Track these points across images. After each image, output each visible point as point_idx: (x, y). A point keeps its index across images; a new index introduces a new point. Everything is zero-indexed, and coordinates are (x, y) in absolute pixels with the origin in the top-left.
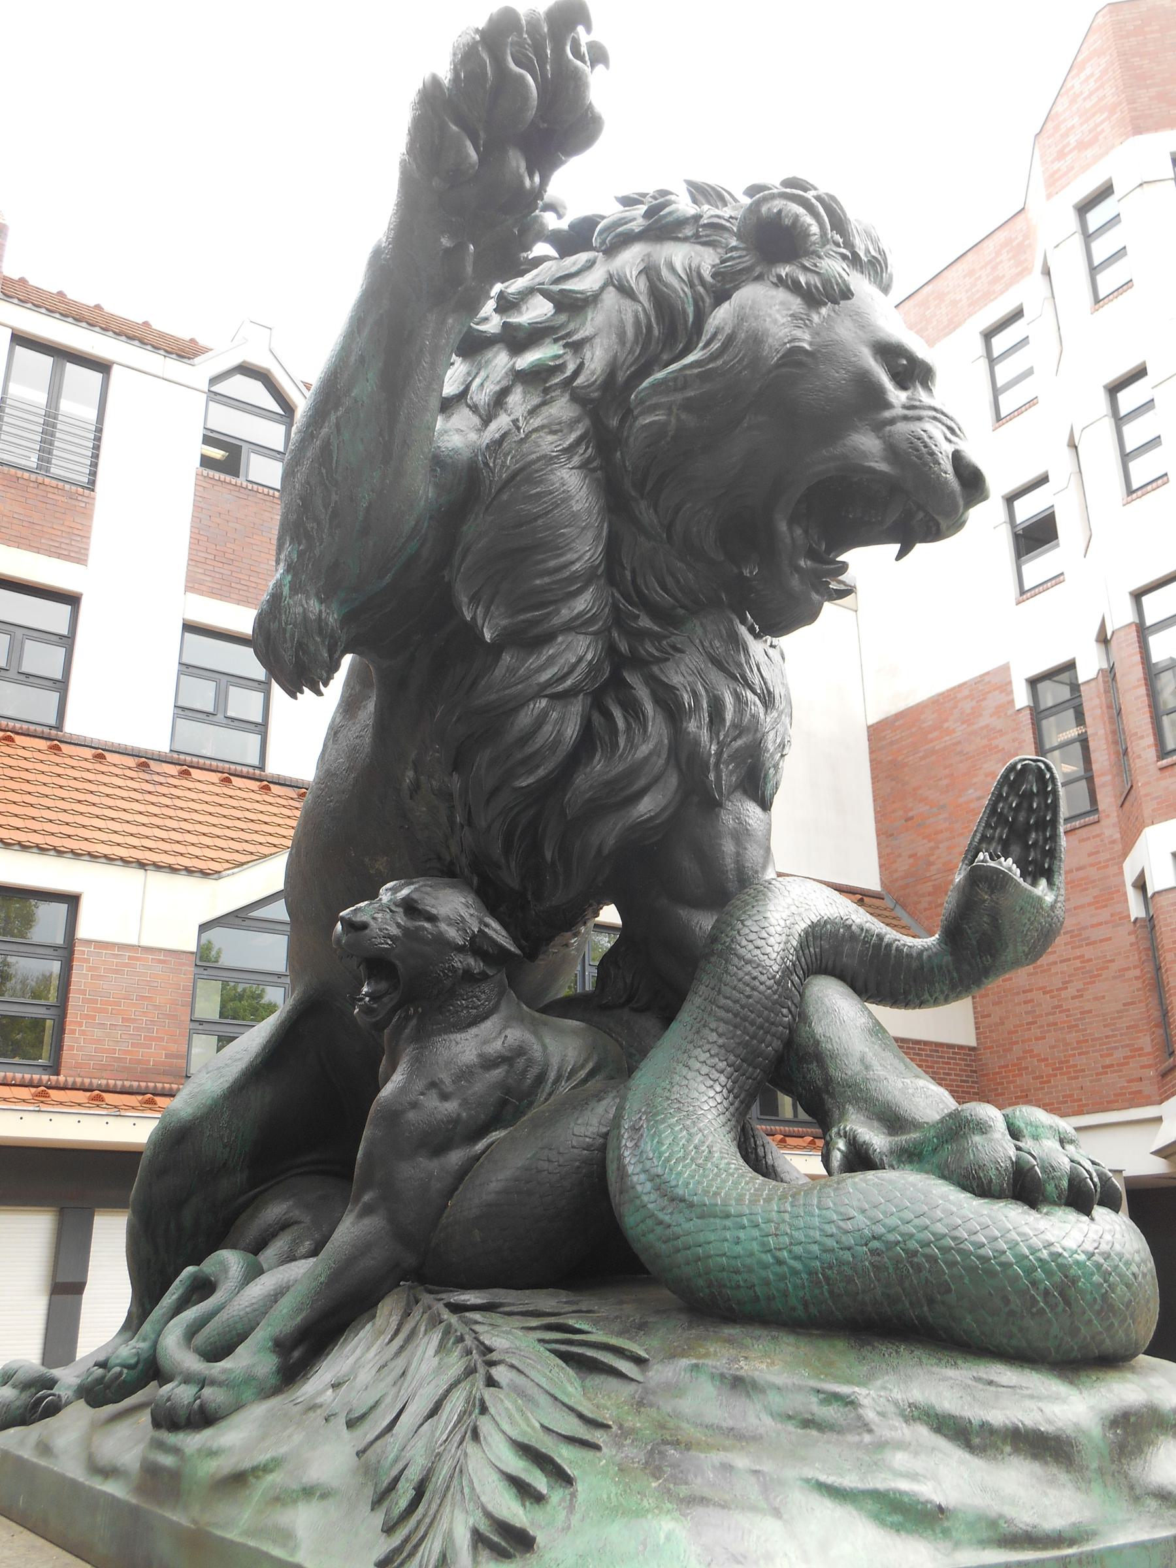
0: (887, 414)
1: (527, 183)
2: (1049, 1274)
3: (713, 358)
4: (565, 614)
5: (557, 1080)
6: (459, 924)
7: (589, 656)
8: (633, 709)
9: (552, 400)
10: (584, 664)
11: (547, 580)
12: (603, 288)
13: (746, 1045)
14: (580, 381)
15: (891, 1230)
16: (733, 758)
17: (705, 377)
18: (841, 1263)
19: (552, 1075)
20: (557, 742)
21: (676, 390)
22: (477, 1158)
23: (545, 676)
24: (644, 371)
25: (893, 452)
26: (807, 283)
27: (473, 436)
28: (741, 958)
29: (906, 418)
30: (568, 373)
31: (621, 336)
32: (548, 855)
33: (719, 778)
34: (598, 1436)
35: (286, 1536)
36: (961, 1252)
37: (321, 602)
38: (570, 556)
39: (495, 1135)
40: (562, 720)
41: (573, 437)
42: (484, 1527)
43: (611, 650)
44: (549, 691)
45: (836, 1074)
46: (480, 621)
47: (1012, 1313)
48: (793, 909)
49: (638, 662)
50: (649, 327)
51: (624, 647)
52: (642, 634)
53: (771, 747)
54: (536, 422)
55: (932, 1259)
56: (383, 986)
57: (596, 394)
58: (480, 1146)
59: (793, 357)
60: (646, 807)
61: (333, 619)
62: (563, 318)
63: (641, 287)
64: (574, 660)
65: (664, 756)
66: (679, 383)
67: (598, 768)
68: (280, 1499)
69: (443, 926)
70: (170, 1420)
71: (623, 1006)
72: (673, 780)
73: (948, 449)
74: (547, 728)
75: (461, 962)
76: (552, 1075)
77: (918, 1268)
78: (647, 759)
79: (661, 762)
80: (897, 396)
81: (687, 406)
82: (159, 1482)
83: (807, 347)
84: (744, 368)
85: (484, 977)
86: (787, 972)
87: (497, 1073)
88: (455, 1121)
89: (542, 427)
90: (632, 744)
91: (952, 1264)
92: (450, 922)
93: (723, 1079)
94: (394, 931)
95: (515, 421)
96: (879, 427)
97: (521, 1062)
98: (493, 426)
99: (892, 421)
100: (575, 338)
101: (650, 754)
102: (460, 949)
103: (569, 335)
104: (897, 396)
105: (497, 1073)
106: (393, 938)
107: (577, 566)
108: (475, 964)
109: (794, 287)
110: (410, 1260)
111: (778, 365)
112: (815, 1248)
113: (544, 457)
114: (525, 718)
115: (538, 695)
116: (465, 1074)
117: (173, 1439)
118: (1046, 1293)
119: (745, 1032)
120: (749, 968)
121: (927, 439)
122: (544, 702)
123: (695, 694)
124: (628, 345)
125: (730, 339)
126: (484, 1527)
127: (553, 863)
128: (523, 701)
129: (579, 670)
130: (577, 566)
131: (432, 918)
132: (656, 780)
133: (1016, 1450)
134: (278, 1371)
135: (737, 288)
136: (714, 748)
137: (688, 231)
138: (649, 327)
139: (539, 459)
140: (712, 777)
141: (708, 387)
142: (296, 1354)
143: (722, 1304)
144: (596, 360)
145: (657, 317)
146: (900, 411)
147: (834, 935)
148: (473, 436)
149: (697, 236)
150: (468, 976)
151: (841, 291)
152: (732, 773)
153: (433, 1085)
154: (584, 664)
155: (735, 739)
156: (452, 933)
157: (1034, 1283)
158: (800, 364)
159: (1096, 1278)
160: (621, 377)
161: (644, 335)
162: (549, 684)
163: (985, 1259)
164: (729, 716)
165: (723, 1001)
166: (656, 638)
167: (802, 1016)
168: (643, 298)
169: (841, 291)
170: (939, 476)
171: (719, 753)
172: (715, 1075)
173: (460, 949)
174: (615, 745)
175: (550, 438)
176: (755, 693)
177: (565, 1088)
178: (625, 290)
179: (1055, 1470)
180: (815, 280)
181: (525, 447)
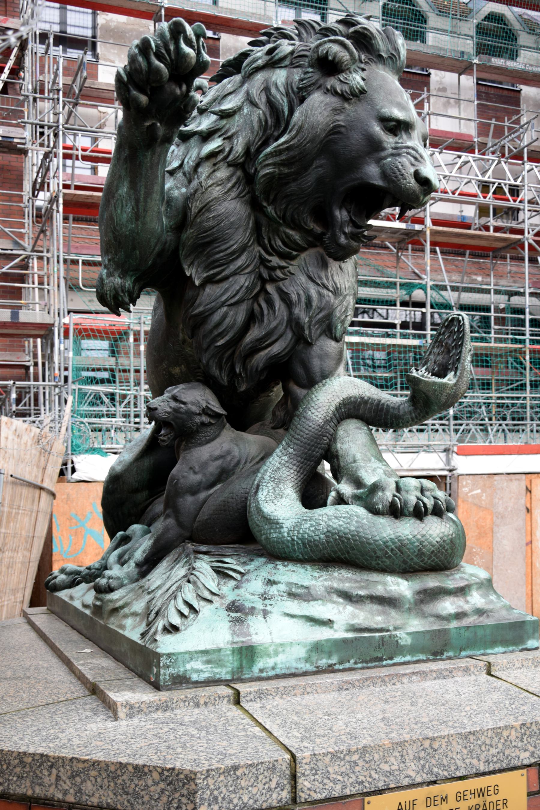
0: (383, 154)
1: (178, 92)
2: (394, 543)
3: (293, 138)
4: (233, 267)
5: (246, 463)
6: (197, 404)
7: (246, 284)
8: (270, 303)
9: (218, 169)
10: (244, 289)
11: (222, 254)
12: (243, 103)
13: (306, 453)
14: (230, 158)
15: (334, 529)
16: (317, 323)
17: (287, 149)
18: (314, 540)
19: (243, 461)
20: (232, 327)
21: (276, 156)
22: (211, 495)
23: (224, 298)
24: (265, 143)
25: (384, 175)
26: (341, 91)
27: (184, 190)
28: (305, 418)
29: (393, 155)
30: (225, 153)
31: (252, 128)
32: (238, 371)
33: (310, 332)
34: (215, 599)
35: (123, 627)
36: (359, 536)
37: (121, 278)
38: (231, 243)
39: (219, 486)
40: (236, 314)
41: (230, 185)
42: (167, 625)
43: (260, 277)
44: (228, 303)
45: (342, 464)
46: (193, 276)
47: (377, 557)
48: (334, 394)
49: (273, 280)
50: (266, 121)
51: (265, 275)
52: (274, 269)
53: (338, 314)
54: (210, 182)
55: (348, 539)
56: (168, 431)
57: (241, 160)
58: (212, 491)
59: (335, 131)
60: (276, 348)
61: (128, 283)
62: (224, 122)
63: (262, 100)
64: (238, 288)
65: (284, 325)
66: (277, 152)
67: (255, 333)
68: (126, 616)
69: (190, 406)
70: (99, 590)
71: (280, 428)
72: (289, 335)
73: (412, 170)
74: (227, 320)
75: (198, 419)
76: (243, 461)
77: (343, 542)
78: (276, 328)
79: (283, 327)
80: (389, 140)
81: (282, 164)
82: (98, 610)
83: (343, 124)
84: (308, 143)
85: (210, 424)
86: (327, 422)
87: (219, 463)
88: (200, 483)
89: (213, 184)
90: (270, 323)
91: (355, 541)
92: (193, 404)
93: (295, 468)
94: (169, 410)
95: (201, 183)
96: (378, 161)
97: (229, 458)
98: (192, 185)
99: (385, 158)
100: (229, 134)
101: (278, 325)
102: (199, 414)
103: (226, 132)
104: (389, 140)
105: (219, 463)
106: (168, 413)
107: (235, 247)
108: (205, 419)
109: (334, 93)
110: (187, 534)
111: (327, 136)
112: (306, 536)
113: (215, 198)
114: (216, 317)
115: (223, 304)
116: (204, 465)
117: (100, 596)
118: (392, 550)
119: (305, 448)
120: (308, 422)
121: (400, 167)
122: (225, 309)
123: (298, 294)
124: (255, 133)
125: (301, 128)
126: (167, 625)
127: (240, 373)
128: (213, 311)
129: (241, 292)
130: (235, 247)
131: (184, 403)
132: (281, 336)
133: (372, 602)
134: (138, 574)
135: (309, 94)
136: (307, 319)
137: (287, 62)
138: (266, 121)
139: (212, 200)
140: (307, 332)
141: (292, 153)
142: (144, 568)
143: (279, 553)
144: (239, 146)
145: (271, 114)
146: (391, 151)
147: (355, 402)
148: (184, 190)
149: (291, 64)
150: (203, 424)
151: (360, 91)
152: (317, 329)
153: (191, 468)
154: (244, 289)
155: (318, 314)
156: (194, 409)
157: (387, 547)
158: (340, 133)
159: (417, 544)
160: (253, 149)
161: (264, 126)
162: (227, 300)
163: (367, 539)
164: (315, 304)
165: (296, 436)
166: (282, 268)
167: (333, 438)
168: (262, 106)
169: (360, 91)
170: (406, 186)
171: (310, 322)
172: (291, 466)
173: (199, 414)
174: (263, 321)
175: (218, 188)
176: (328, 289)
177: (249, 465)
178: (254, 104)
179: (387, 608)
180: (346, 88)
181: (206, 196)
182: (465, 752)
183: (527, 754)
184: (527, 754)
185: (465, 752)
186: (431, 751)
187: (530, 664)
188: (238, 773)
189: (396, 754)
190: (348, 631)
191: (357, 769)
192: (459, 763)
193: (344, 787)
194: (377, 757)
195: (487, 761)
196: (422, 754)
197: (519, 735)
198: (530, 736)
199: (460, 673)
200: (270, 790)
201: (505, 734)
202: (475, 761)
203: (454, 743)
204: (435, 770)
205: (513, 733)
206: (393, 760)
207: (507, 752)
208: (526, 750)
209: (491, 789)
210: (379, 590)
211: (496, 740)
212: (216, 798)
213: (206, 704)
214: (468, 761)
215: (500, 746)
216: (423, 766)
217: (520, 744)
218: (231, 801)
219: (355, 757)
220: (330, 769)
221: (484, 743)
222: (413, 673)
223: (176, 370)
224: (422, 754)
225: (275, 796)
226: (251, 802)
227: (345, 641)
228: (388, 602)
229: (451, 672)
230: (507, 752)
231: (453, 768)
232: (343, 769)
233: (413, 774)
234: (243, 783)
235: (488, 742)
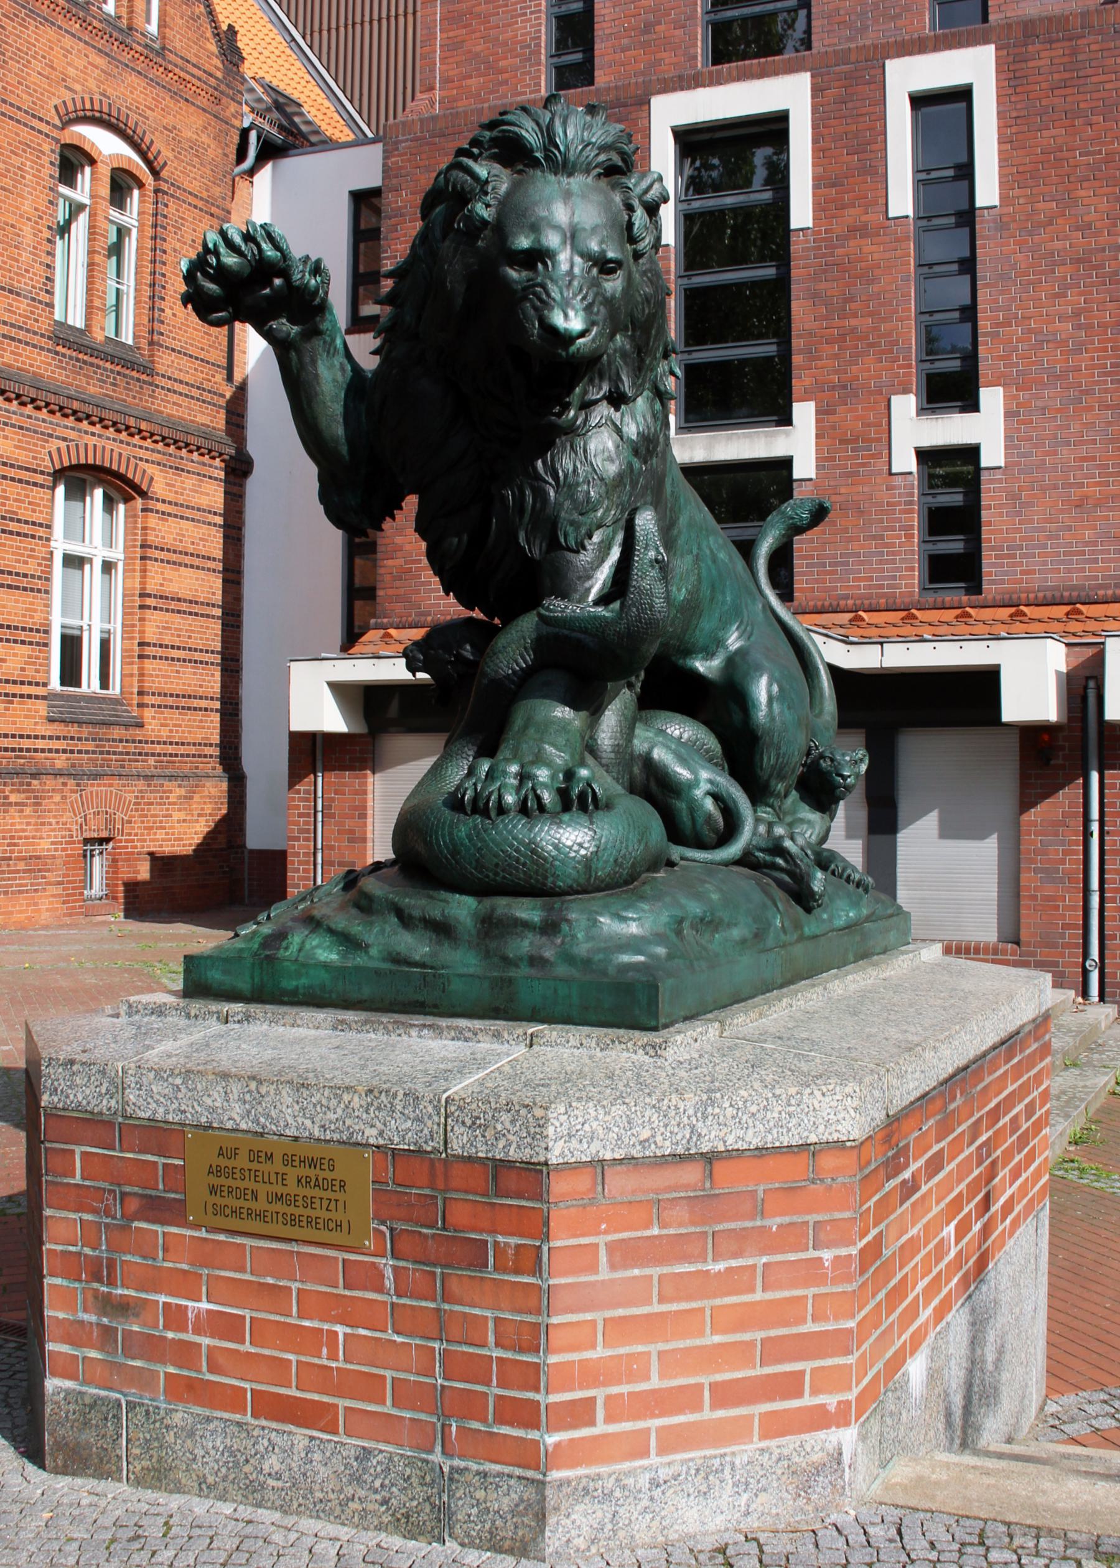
133: (426, 928)
182: (297, 1107)
183: (374, 1132)
184: (374, 1132)
185: (297, 1107)
186: (255, 1094)
187: (593, 1045)
188: (75, 1068)
189: (219, 1088)
190: (384, 960)
191: (180, 1095)
192: (290, 1120)
193: (167, 1112)
194: (199, 1087)
195: (323, 1126)
196: (248, 1097)
197: (364, 1103)
198: (379, 1108)
199: (488, 1038)
200: (100, 1094)
201: (346, 1097)
202: (308, 1123)
203: (284, 1093)
204: (262, 1120)
205: (356, 1099)
206: (216, 1095)
207: (348, 1122)
208: (372, 1126)
209: (325, 1162)
210: (436, 913)
211: (334, 1102)
212: (56, 1090)
213: (196, 1016)
214: (300, 1120)
215: (339, 1111)
216: (249, 1112)
217: (365, 1116)
218: (67, 1097)
219: (178, 1081)
220: (154, 1088)
221: (320, 1102)
222: (424, 1026)
223: (1046, 737)
224: (248, 1097)
225: (105, 1102)
226: (84, 1102)
227: (377, 972)
228: (442, 929)
229: (476, 1034)
230: (348, 1122)
231: (282, 1124)
232: (166, 1091)
233: (238, 1119)
234: (78, 1082)
235: (324, 1102)
